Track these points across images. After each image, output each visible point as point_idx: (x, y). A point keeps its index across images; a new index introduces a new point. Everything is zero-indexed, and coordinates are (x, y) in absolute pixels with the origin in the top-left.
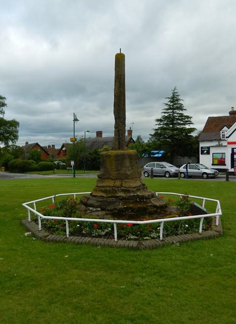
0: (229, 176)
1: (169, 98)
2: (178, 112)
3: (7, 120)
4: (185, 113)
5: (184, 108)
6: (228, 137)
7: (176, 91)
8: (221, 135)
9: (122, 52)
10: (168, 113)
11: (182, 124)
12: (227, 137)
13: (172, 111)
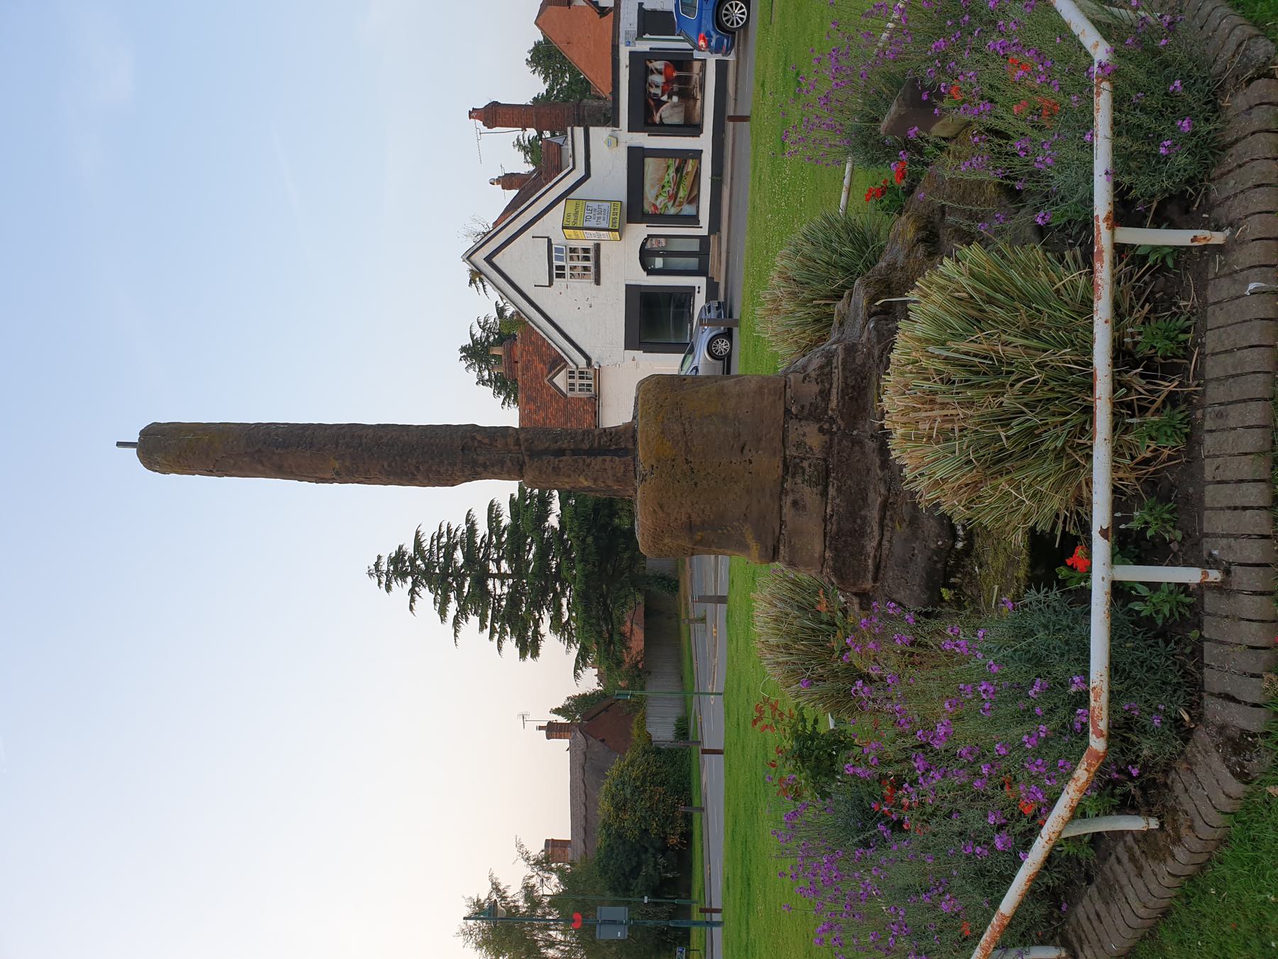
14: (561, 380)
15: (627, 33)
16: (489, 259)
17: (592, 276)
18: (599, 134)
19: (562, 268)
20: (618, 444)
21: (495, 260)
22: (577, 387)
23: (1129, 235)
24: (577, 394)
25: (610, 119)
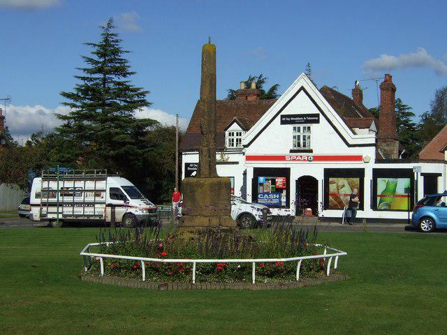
0: (331, 179)
1: (95, 45)
2: (116, 79)
3: (164, 125)
4: (133, 81)
5: (130, 70)
6: (245, 146)
7: (111, 31)
8: (227, 141)
9: (373, 141)
10: (91, 80)
11: (125, 108)
12: (245, 146)
13: (101, 76)
14: (235, 127)
15: (420, 167)
16: (302, 88)
17: (295, 148)
18: (370, 153)
19: (299, 131)
20: (212, 171)
21: (302, 91)
22: (231, 137)
23: (254, 264)
24: (227, 138)
25: (378, 160)
